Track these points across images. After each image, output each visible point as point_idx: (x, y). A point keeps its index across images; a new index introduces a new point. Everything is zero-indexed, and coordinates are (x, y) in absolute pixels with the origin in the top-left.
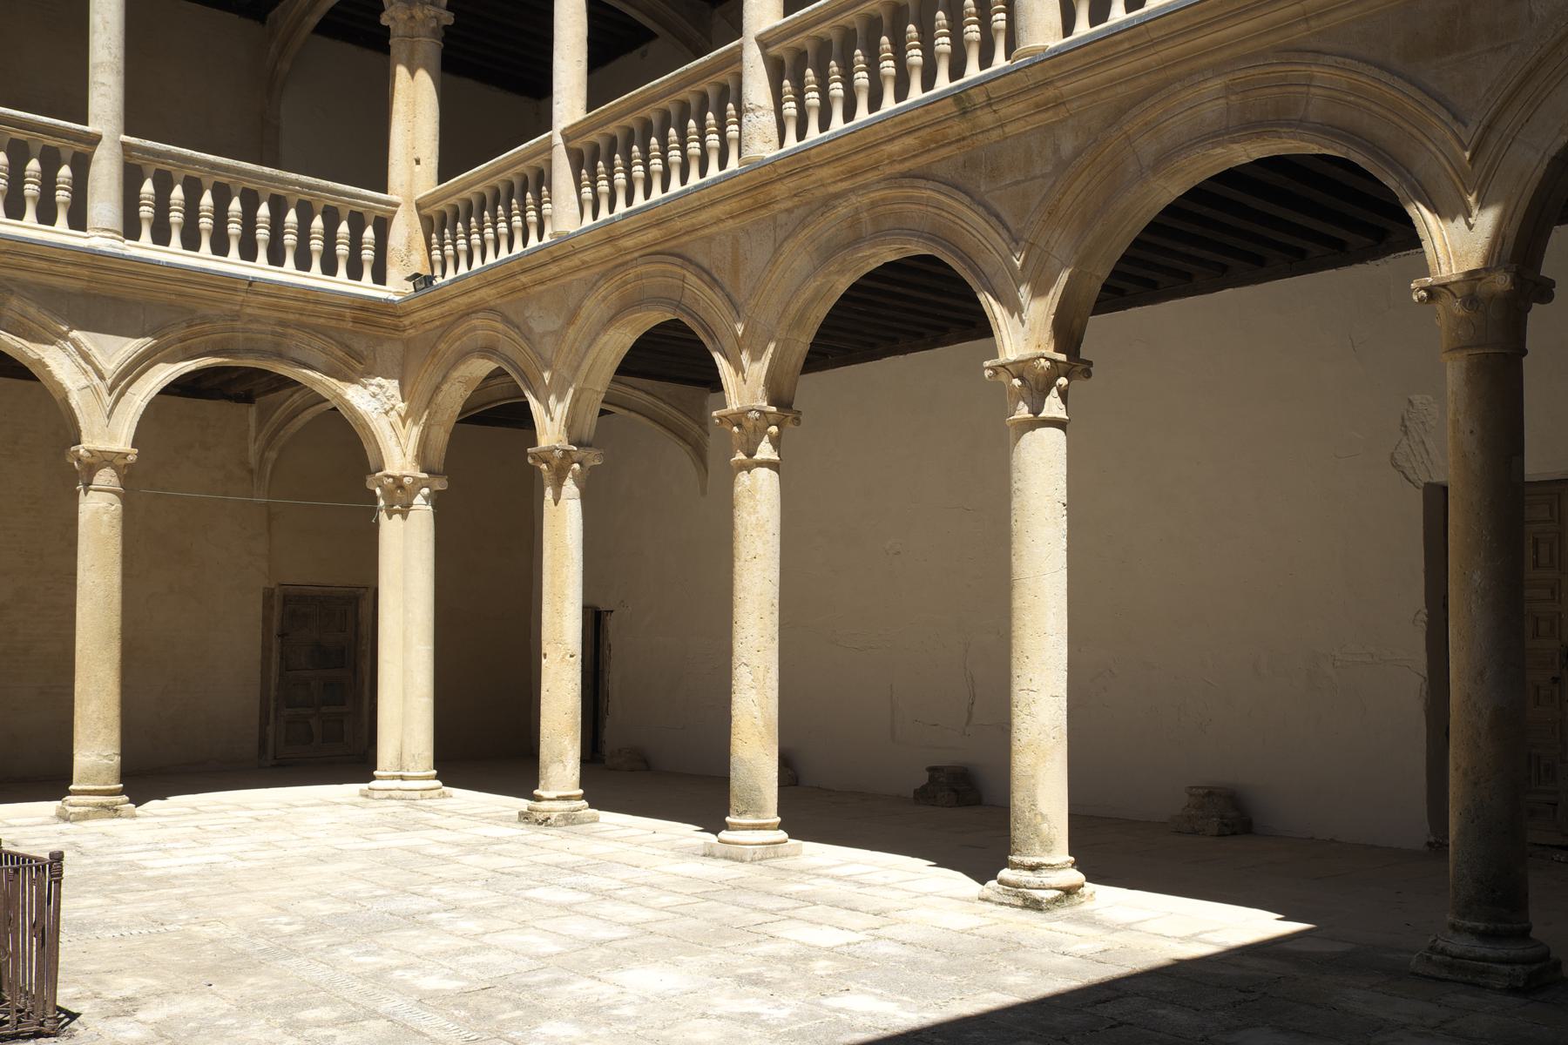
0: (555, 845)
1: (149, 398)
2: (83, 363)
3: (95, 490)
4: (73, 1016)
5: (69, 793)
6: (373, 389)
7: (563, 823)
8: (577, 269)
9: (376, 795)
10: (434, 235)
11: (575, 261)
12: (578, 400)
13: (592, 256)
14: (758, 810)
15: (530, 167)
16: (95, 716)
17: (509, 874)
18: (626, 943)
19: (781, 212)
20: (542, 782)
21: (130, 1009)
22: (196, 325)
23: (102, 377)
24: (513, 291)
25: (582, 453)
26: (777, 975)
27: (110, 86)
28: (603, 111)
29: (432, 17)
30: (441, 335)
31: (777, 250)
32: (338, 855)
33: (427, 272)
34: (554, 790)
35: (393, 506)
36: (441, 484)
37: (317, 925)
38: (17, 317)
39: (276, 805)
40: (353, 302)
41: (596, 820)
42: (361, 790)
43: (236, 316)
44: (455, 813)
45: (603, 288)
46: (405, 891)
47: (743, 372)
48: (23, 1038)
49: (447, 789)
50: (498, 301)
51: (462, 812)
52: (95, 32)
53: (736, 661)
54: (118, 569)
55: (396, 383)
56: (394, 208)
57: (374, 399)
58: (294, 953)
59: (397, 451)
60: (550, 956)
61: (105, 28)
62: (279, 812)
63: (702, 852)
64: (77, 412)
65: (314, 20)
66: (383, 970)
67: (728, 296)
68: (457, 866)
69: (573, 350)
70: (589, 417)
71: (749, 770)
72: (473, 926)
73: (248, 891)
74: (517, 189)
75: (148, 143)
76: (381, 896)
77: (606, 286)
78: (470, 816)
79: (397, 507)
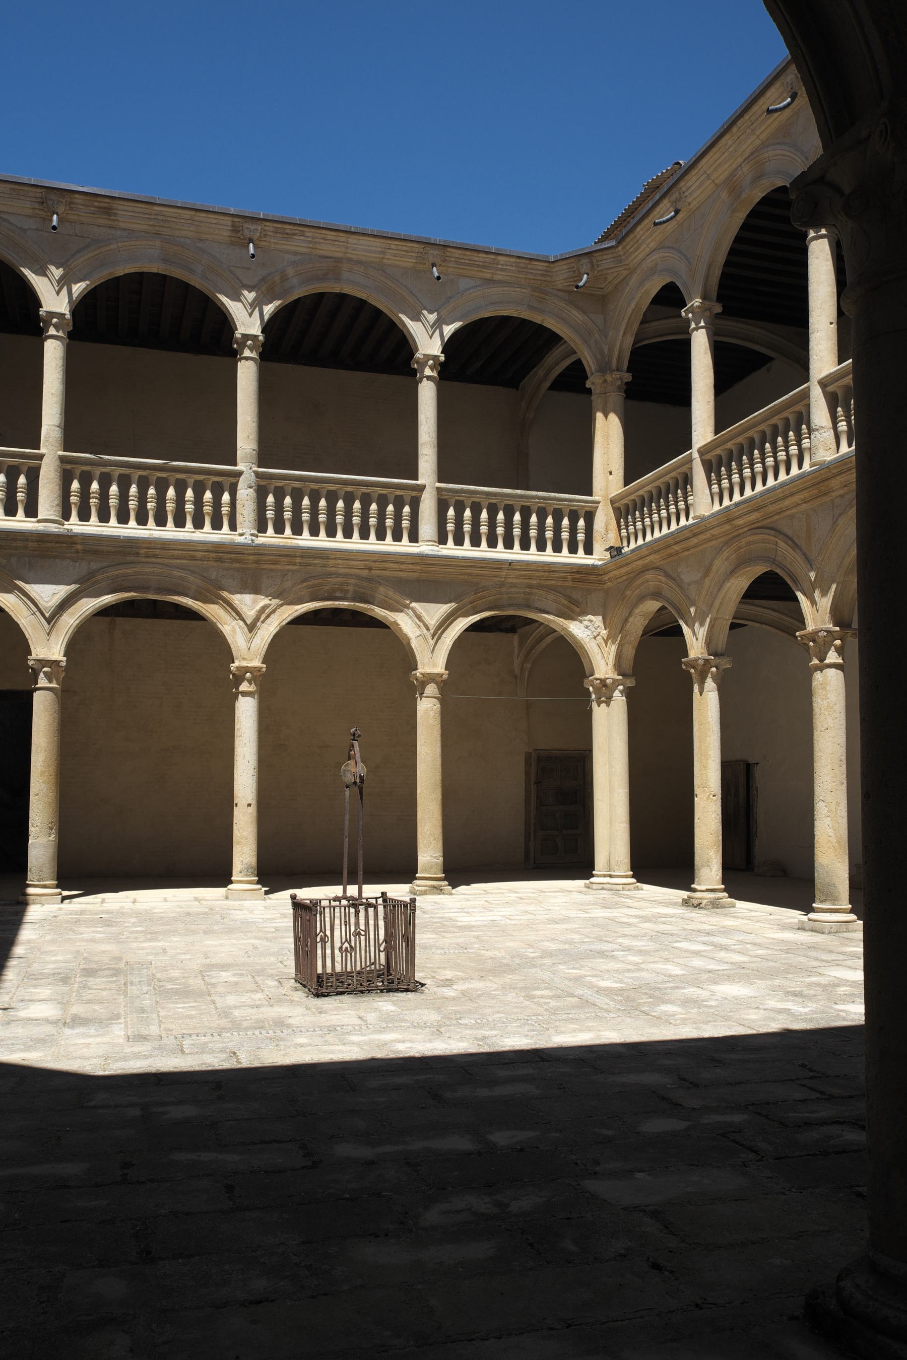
0: (703, 919)
1: (454, 640)
2: (417, 621)
3: (426, 697)
4: (423, 985)
5: (416, 879)
6: (586, 623)
7: (710, 907)
8: (709, 540)
9: (594, 886)
10: (622, 520)
11: (708, 535)
12: (713, 626)
13: (718, 531)
14: (834, 899)
15: (679, 473)
16: (428, 833)
17: (666, 934)
18: (725, 972)
19: (837, 497)
20: (696, 880)
21: (449, 984)
22: (480, 592)
23: (428, 629)
24: (670, 556)
25: (718, 660)
26: (812, 992)
27: (430, 456)
28: (723, 435)
29: (617, 379)
30: (627, 586)
31: (835, 523)
32: (566, 920)
33: (618, 545)
34: (704, 885)
35: (600, 698)
36: (631, 683)
37: (550, 954)
38: (383, 597)
39: (533, 891)
40: (572, 568)
41: (733, 906)
42: (585, 884)
43: (502, 585)
44: (643, 899)
45: (725, 552)
46: (601, 940)
47: (816, 605)
48: (401, 991)
49: (638, 884)
50: (661, 563)
51: (646, 898)
52: (421, 425)
53: (816, 799)
54: (439, 744)
55: (600, 618)
56: (597, 505)
57: (586, 630)
58: (534, 966)
59: (602, 662)
60: (677, 975)
61: (427, 422)
62: (534, 895)
63: (796, 927)
64: (415, 651)
65: (548, 384)
66: (581, 977)
67: (804, 554)
68: (636, 928)
69: (709, 593)
70: (722, 636)
71: (827, 872)
72: (637, 959)
73: (513, 936)
74: (672, 488)
75: (451, 486)
76: (587, 942)
77: (727, 550)
78: (652, 901)
79: (603, 699)
